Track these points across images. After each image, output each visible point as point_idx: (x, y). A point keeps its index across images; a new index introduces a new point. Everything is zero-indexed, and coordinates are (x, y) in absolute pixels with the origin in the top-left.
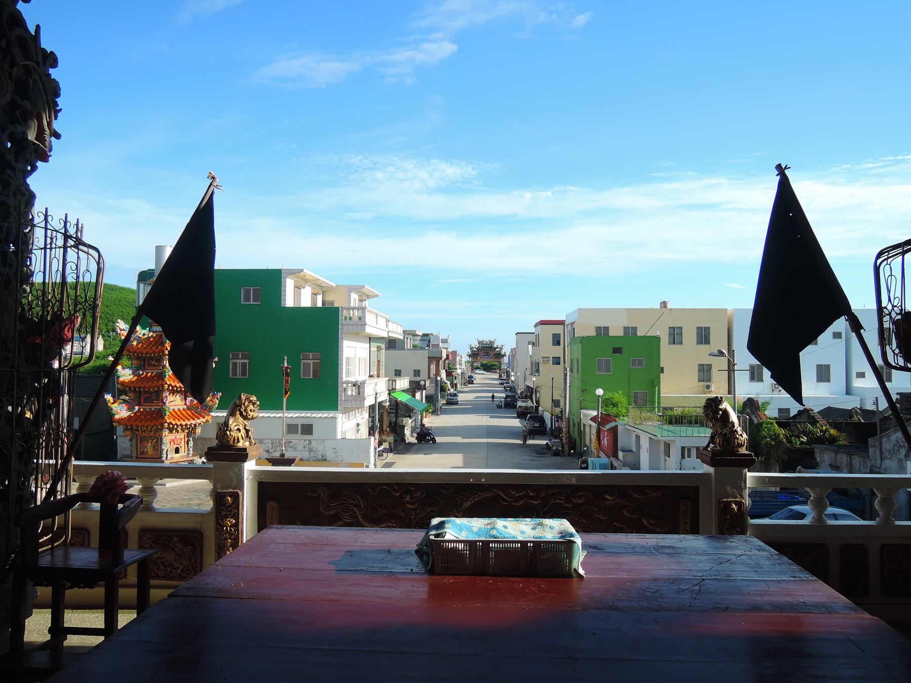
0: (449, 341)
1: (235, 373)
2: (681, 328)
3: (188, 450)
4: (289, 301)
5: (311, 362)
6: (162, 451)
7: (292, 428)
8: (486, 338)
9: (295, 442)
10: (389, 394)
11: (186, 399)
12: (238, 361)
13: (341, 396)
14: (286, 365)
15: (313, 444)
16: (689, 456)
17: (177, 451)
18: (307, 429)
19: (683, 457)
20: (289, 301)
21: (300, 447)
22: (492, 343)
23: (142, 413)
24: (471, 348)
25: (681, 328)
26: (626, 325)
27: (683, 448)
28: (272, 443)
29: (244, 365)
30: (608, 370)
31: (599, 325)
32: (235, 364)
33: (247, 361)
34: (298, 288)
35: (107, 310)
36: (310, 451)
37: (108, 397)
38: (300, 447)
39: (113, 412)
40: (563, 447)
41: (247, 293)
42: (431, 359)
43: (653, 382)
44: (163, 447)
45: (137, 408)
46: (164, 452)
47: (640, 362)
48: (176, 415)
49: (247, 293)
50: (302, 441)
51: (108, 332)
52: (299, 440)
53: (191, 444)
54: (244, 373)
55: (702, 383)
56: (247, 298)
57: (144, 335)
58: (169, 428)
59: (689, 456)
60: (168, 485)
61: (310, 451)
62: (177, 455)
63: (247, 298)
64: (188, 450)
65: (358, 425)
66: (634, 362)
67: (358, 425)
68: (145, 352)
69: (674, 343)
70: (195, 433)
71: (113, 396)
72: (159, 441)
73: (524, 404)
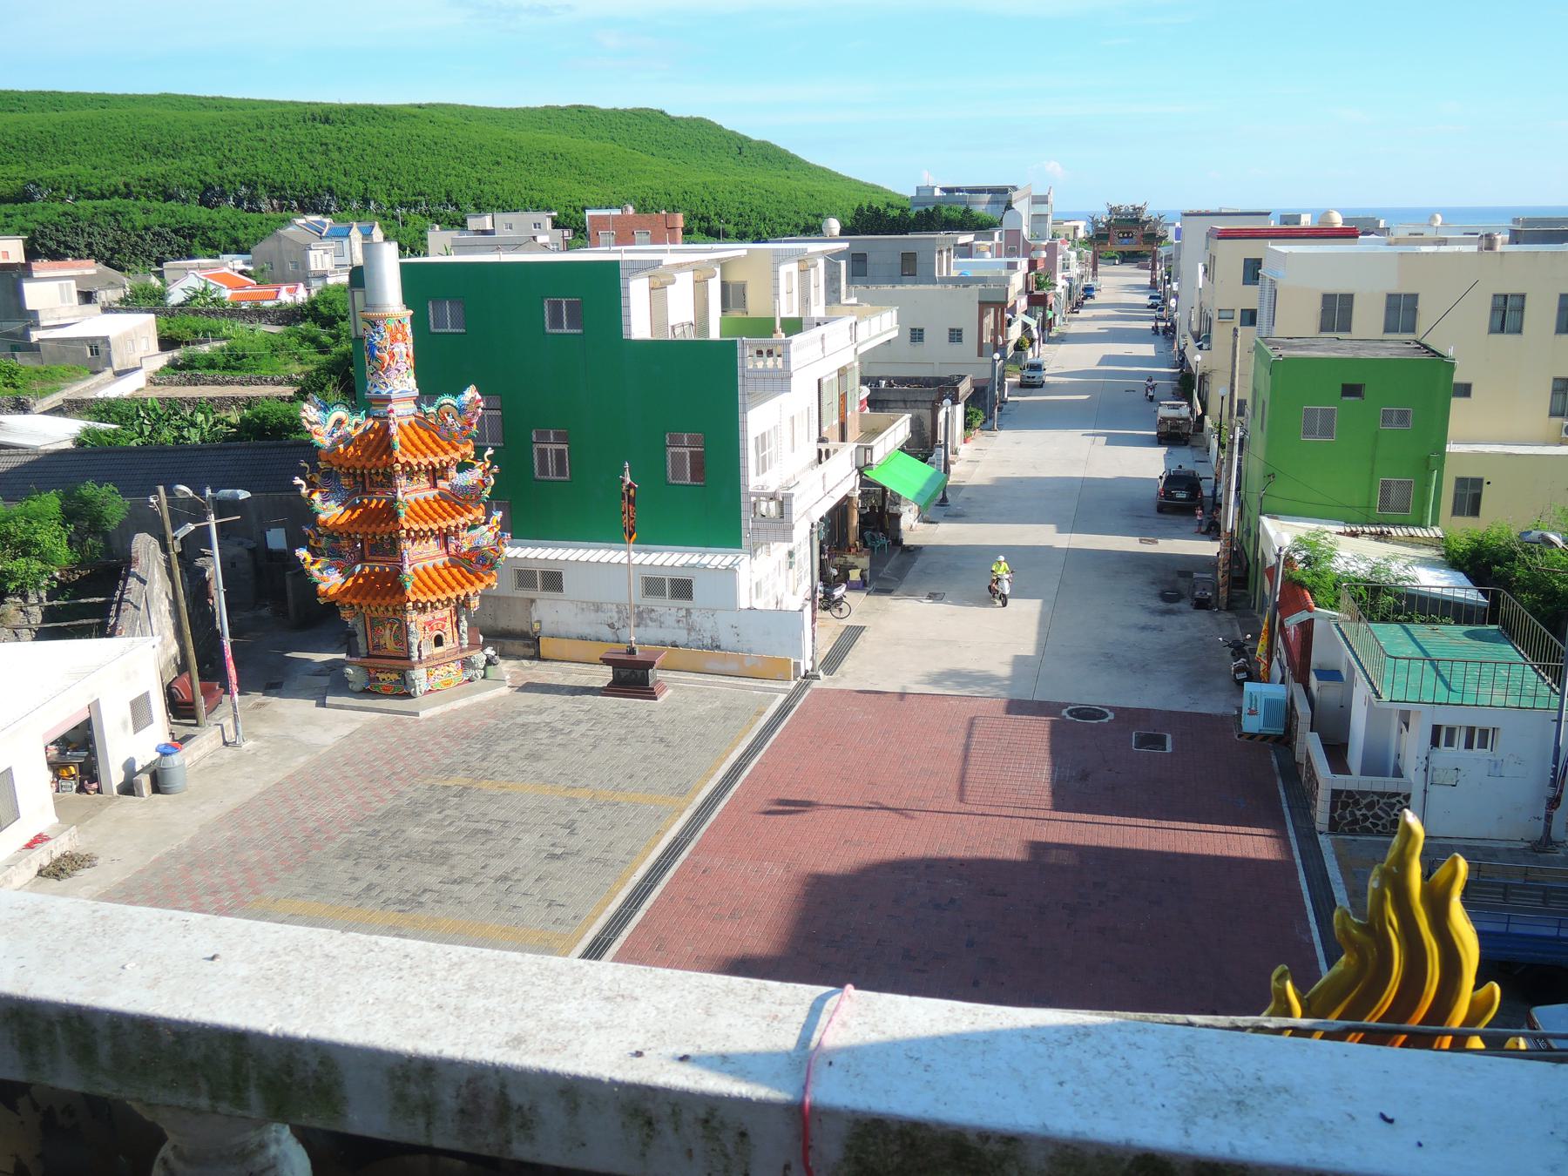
0: (1050, 199)
1: (544, 470)
2: (1523, 296)
3: (460, 638)
4: (639, 327)
5: (687, 450)
6: (409, 646)
7: (653, 586)
8: (1126, 200)
9: (660, 610)
10: (861, 473)
11: (447, 547)
12: (549, 447)
13: (747, 522)
14: (628, 480)
15: (695, 616)
16: (1449, 743)
17: (439, 641)
18: (682, 589)
19: (1435, 742)
20: (639, 327)
21: (670, 621)
22: (1138, 210)
23: (366, 577)
24: (1094, 223)
25: (1523, 296)
26: (1394, 289)
27: (1436, 730)
28: (619, 612)
29: (560, 453)
30: (1327, 431)
31: (1331, 290)
32: (543, 453)
33: (565, 447)
34: (658, 290)
35: (387, 163)
36: (690, 629)
37: (302, 553)
38: (670, 621)
39: (315, 579)
40: (1216, 590)
41: (556, 307)
42: (984, 305)
43: (1427, 460)
44: (412, 639)
45: (358, 568)
46: (415, 648)
47: (1403, 417)
48: (429, 580)
49: (556, 307)
50: (673, 611)
51: (392, 207)
52: (666, 607)
53: (464, 625)
54: (561, 471)
55: (1558, 420)
56: (557, 322)
57: (357, 425)
58: (415, 607)
59: (1449, 743)
60: (423, 714)
61: (690, 629)
62: (440, 650)
63: (557, 322)
64: (460, 638)
65: (791, 554)
66: (1386, 417)
67: (791, 554)
68: (358, 465)
69: (1502, 330)
70: (468, 607)
71: (312, 551)
72: (403, 633)
73: (1173, 413)
